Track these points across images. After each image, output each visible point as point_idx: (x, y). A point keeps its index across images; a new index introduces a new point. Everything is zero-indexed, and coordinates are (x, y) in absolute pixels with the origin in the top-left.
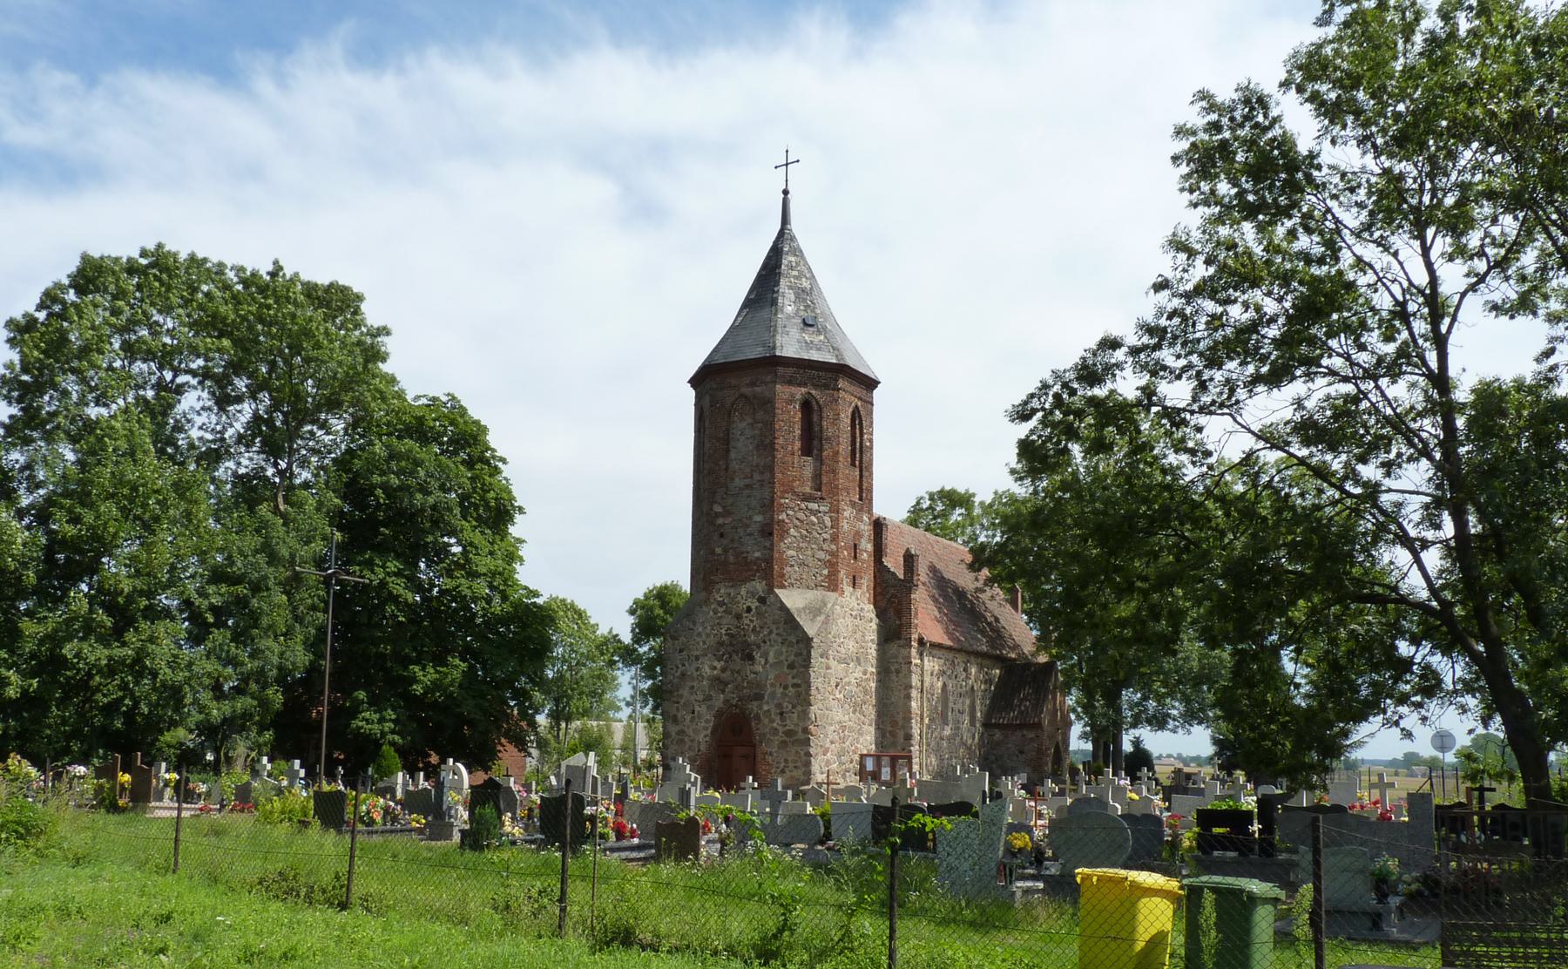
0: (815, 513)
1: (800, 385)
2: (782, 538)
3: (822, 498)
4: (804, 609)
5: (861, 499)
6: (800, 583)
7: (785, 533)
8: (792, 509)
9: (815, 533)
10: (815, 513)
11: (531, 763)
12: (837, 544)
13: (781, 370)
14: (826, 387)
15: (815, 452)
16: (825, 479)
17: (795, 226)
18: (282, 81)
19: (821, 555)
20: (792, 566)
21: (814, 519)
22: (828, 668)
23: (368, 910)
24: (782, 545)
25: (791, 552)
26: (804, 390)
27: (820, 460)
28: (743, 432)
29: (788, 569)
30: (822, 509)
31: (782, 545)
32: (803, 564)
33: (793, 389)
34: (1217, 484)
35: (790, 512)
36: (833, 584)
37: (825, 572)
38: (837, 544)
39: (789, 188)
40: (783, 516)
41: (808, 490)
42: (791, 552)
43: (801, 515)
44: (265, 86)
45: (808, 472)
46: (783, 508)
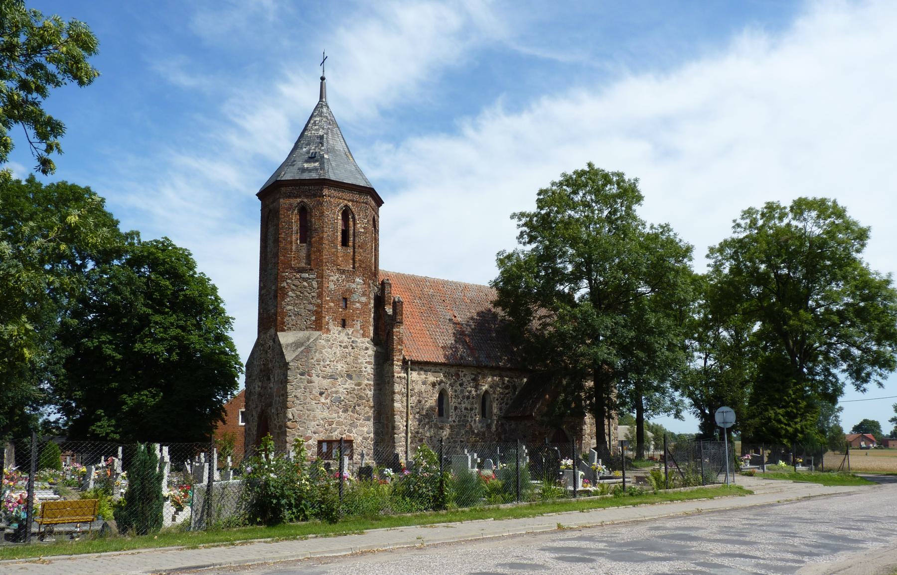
0: (305, 280)
1: (296, 197)
2: (283, 299)
3: (311, 270)
4: (292, 344)
5: (354, 268)
6: (296, 327)
7: (285, 295)
8: (290, 279)
9: (306, 294)
10: (305, 280)
11: (14, 469)
12: (321, 299)
13: (283, 189)
14: (315, 196)
15: (308, 239)
16: (313, 257)
17: (330, 99)
18: (476, 128)
19: (311, 307)
20: (290, 316)
21: (305, 284)
22: (310, 382)
23: (365, 517)
24: (283, 303)
25: (289, 307)
26: (299, 200)
27: (310, 245)
28: (271, 229)
29: (287, 318)
30: (311, 276)
31: (283, 303)
32: (297, 314)
33: (292, 201)
34: (656, 242)
35: (288, 281)
36: (318, 325)
37: (313, 318)
38: (321, 299)
39: (326, 76)
40: (285, 284)
41: (303, 265)
42: (289, 307)
43: (297, 282)
44: (469, 131)
45: (303, 253)
46: (284, 279)
